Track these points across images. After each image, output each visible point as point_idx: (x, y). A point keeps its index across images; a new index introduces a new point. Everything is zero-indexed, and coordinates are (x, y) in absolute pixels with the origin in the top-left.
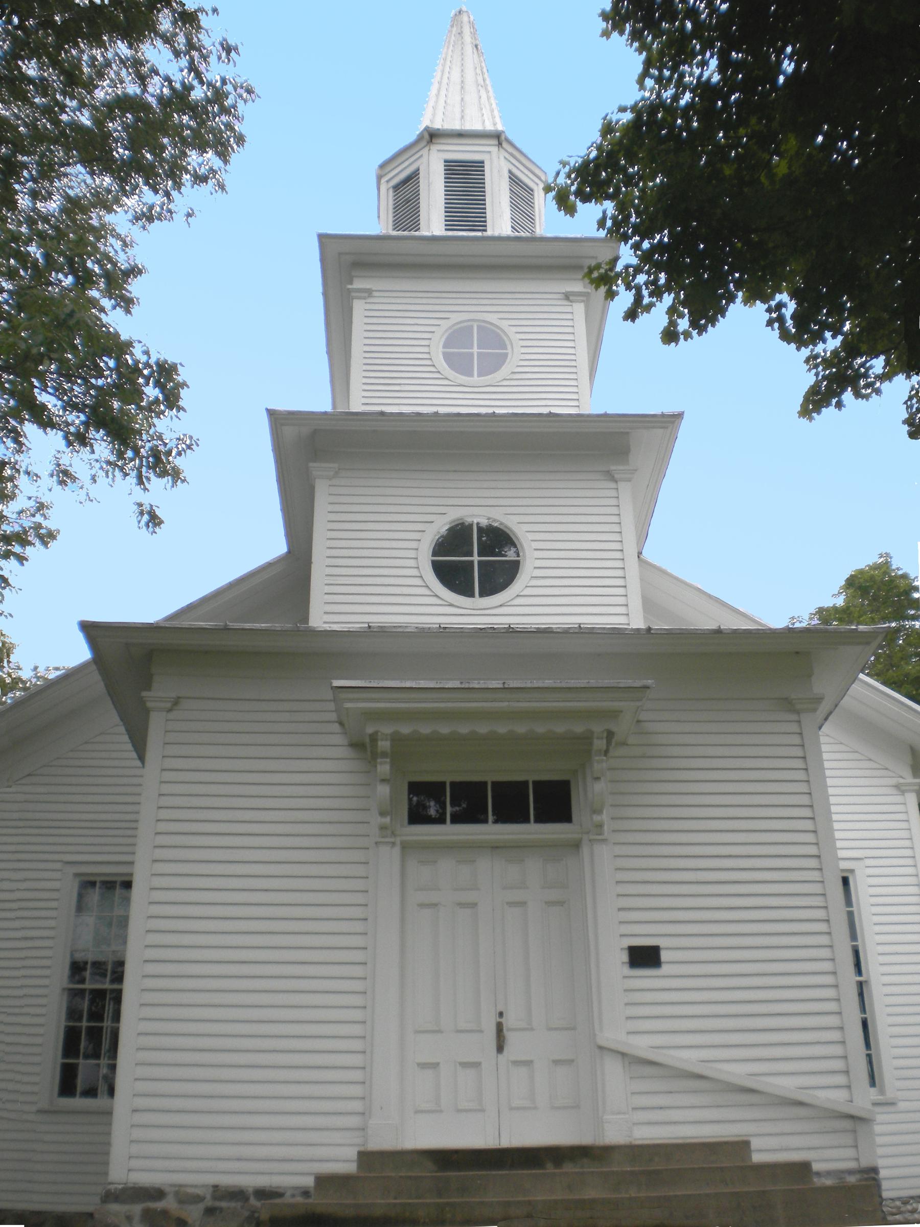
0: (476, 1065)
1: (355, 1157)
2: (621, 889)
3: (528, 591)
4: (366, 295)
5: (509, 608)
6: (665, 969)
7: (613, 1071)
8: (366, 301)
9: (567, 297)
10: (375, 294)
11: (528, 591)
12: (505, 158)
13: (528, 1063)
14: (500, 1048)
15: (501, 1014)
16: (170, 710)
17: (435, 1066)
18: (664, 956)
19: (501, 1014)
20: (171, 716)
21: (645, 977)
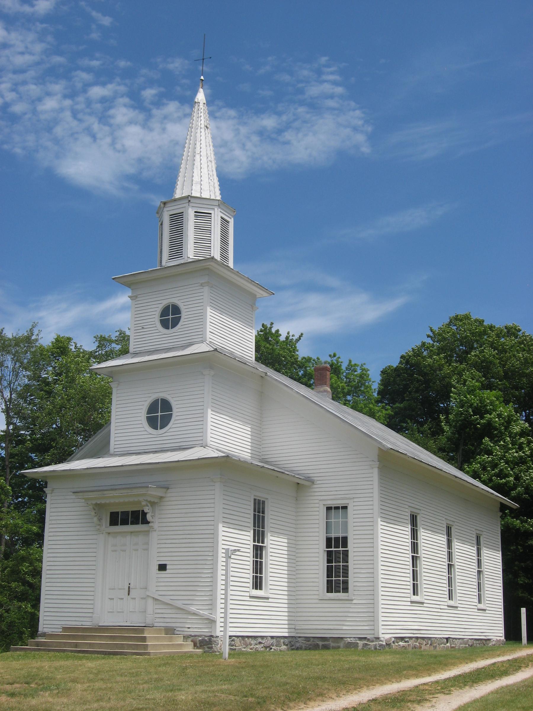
0: (122, 599)
1: (167, 570)
2: (159, 546)
3: (174, 426)
4: (134, 298)
5: (168, 433)
6: (168, 571)
7: (150, 601)
8: (136, 300)
9: (202, 285)
10: (138, 296)
11: (174, 426)
12: (220, 211)
13: (135, 599)
14: (129, 594)
15: (130, 584)
16: (51, 493)
17: (113, 599)
18: (168, 567)
19: (130, 584)
20: (52, 494)
21: (163, 574)
